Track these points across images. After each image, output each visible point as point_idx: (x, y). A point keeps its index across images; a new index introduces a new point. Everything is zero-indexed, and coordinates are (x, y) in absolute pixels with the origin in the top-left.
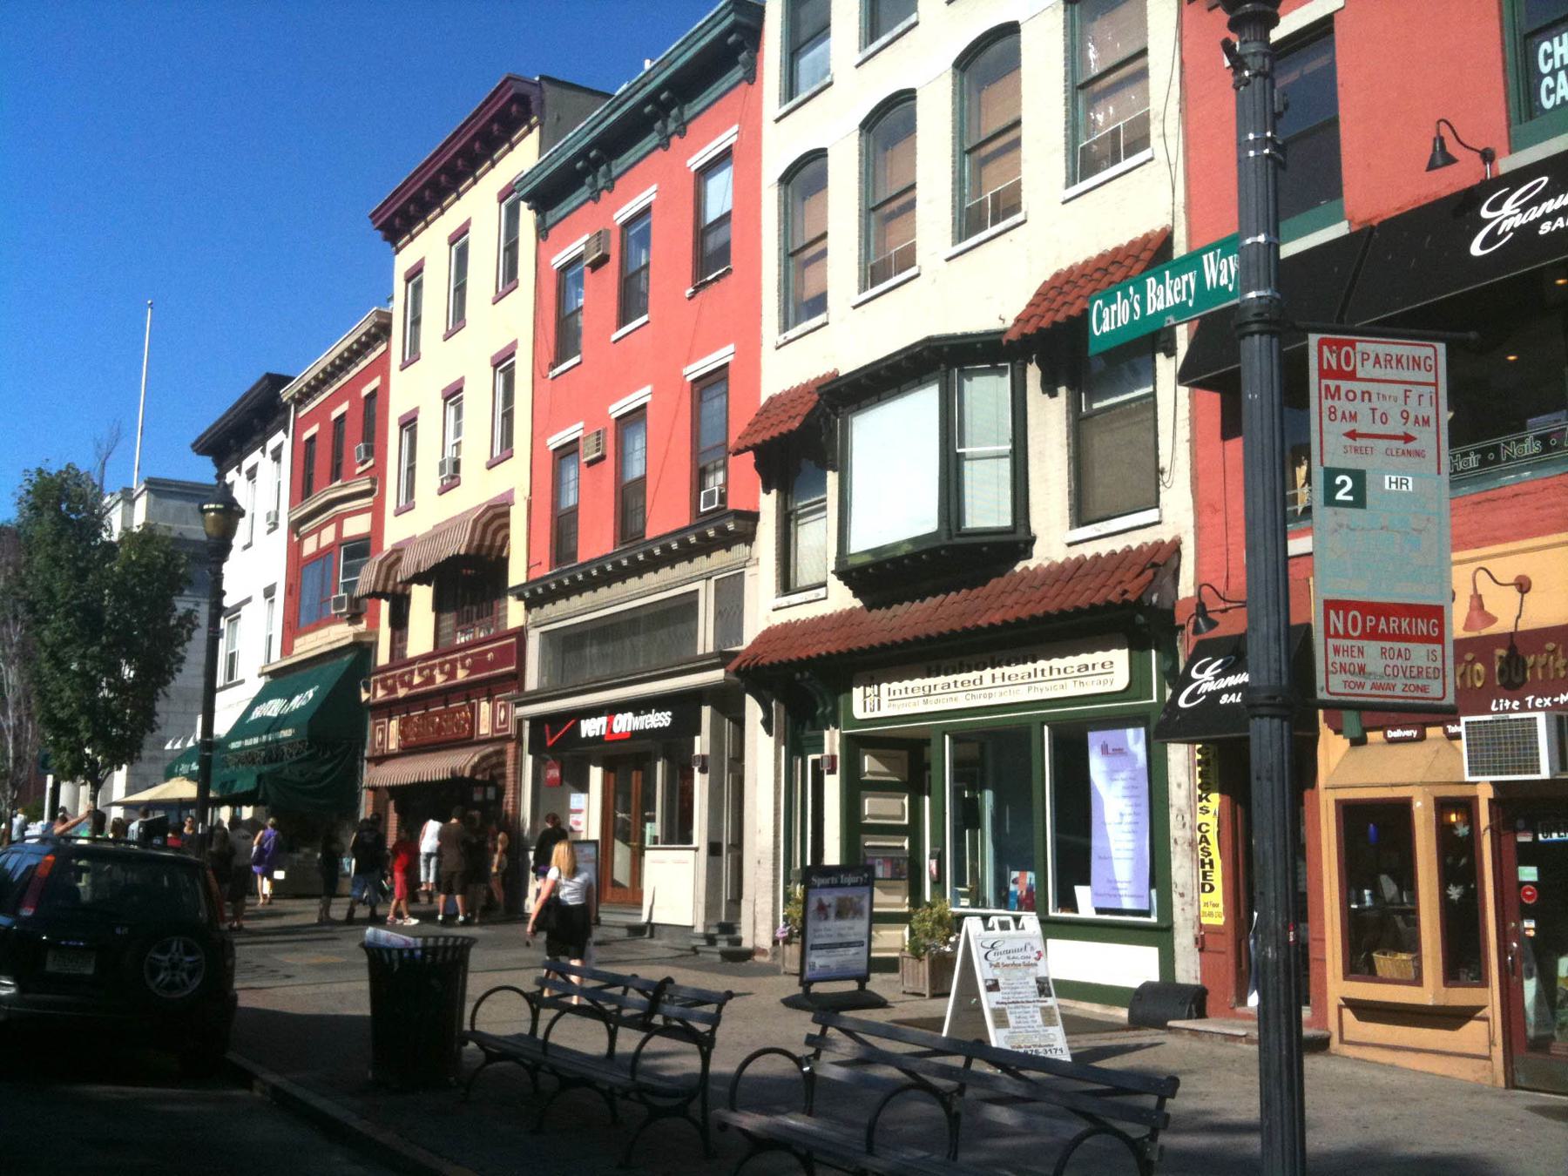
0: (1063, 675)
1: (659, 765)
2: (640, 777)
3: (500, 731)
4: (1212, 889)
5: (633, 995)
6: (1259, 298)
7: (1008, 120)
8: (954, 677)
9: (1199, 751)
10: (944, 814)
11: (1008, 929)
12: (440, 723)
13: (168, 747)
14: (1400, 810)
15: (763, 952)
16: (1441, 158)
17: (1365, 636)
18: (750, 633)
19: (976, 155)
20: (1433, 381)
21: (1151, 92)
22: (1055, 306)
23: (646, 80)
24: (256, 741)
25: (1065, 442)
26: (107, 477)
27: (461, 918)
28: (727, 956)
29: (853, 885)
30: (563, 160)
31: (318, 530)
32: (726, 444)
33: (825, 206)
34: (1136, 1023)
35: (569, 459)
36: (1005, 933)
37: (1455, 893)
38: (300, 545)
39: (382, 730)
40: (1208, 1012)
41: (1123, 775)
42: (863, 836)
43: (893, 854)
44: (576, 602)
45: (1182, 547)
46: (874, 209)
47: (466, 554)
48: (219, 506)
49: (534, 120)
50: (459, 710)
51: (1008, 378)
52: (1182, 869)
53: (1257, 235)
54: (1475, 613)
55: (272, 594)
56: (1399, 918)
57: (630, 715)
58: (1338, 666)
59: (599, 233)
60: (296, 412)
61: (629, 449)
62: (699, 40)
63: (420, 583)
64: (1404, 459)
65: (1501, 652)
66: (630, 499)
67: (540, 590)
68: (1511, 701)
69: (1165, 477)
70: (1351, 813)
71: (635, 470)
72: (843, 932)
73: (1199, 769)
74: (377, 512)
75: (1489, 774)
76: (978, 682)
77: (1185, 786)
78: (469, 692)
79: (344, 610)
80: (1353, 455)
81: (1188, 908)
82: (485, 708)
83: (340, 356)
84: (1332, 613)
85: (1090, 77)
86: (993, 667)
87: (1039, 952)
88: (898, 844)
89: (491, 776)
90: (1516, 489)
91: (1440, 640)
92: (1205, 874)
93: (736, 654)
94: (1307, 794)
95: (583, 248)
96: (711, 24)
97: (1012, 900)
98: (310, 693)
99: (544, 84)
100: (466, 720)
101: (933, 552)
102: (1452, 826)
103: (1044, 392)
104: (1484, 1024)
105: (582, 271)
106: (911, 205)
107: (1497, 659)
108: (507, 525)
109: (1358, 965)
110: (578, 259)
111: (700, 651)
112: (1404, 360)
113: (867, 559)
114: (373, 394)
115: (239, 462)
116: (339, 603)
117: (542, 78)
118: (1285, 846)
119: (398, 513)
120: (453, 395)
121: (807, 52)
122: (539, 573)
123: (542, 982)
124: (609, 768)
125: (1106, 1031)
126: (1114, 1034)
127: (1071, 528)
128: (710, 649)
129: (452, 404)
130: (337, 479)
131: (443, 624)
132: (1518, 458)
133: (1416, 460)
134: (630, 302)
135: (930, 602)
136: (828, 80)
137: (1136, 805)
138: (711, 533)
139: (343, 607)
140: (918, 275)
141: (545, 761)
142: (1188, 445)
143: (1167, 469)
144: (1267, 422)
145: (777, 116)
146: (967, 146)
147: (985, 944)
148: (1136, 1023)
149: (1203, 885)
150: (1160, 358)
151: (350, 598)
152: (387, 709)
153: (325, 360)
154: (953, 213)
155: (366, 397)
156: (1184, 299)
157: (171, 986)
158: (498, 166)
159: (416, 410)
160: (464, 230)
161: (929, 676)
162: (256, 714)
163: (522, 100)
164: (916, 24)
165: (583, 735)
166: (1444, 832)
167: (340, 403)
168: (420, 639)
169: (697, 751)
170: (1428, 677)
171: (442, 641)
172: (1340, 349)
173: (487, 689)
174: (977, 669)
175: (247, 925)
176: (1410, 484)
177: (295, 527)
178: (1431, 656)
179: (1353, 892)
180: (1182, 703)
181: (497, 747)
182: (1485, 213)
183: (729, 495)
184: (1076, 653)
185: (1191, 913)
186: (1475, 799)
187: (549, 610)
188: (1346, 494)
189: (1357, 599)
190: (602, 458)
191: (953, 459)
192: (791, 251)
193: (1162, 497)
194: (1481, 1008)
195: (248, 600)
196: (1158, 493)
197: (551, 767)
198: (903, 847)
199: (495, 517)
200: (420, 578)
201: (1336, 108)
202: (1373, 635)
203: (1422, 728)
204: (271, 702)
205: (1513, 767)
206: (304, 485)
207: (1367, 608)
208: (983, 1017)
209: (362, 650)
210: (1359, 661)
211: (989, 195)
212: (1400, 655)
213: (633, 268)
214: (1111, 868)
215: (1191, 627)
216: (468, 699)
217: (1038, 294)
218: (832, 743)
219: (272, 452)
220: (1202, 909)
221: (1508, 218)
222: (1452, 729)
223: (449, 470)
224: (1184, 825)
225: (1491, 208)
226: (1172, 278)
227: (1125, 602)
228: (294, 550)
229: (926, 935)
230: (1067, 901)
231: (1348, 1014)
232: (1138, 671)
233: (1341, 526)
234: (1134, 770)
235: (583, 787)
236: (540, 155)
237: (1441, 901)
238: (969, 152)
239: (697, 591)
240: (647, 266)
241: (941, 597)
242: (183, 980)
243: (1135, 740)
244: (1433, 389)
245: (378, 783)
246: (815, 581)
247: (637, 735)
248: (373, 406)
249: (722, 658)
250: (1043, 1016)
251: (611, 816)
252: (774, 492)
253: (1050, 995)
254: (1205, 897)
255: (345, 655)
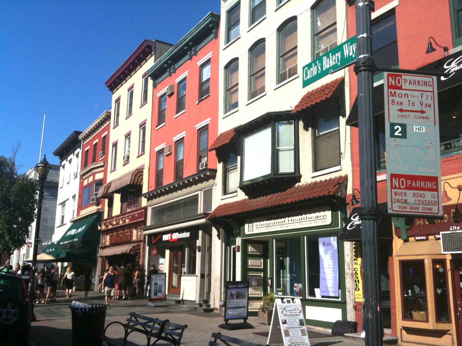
0: (310, 219)
1: (186, 249)
2: (181, 253)
3: (138, 239)
4: (359, 290)
5: (157, 326)
6: (364, 57)
7: (294, 46)
8: (276, 220)
9: (354, 244)
10: (273, 265)
11: (290, 303)
12: (121, 237)
13: (43, 244)
14: (421, 263)
15: (217, 309)
16: (431, 49)
17: (406, 188)
18: (214, 207)
19: (284, 57)
20: (432, 90)
21: (338, 35)
22: (307, 102)
23: (185, 39)
24: (67, 242)
25: (311, 145)
26: (16, 158)
27: (124, 298)
28: (205, 310)
29: (242, 288)
30: (161, 64)
31: (88, 178)
32: (208, 148)
33: (238, 75)
34: (334, 334)
35: (161, 154)
36: (289, 304)
37: (439, 291)
38: (83, 183)
39: (105, 239)
40: (358, 331)
41: (330, 252)
42: (248, 272)
43: (258, 278)
44: (162, 198)
45: (348, 178)
46: (253, 75)
47: (130, 184)
48: (43, 165)
49: (153, 53)
50: (128, 232)
51: (293, 125)
52: (349, 283)
53: (363, 34)
54: (444, 197)
55: (75, 197)
56: (420, 300)
57: (177, 233)
58: (396, 200)
59: (171, 86)
60: (83, 142)
61: (179, 150)
62: (201, 26)
63: (117, 193)
64: (422, 120)
65: (453, 210)
66: (179, 166)
67: (151, 195)
68: (457, 227)
69: (342, 156)
70: (405, 265)
71: (180, 157)
72: (239, 303)
73: (354, 250)
74: (105, 172)
75: (450, 251)
76: (284, 222)
77: (350, 256)
78: (130, 226)
79: (95, 202)
80: (401, 118)
81: (351, 296)
82: (135, 231)
83: (96, 125)
84: (394, 179)
85: (319, 31)
86: (288, 217)
87: (300, 311)
88: (260, 275)
89: (136, 253)
90: (457, 157)
91: (437, 190)
92: (356, 285)
93: (209, 214)
94: (390, 258)
95: (166, 91)
96: (204, 21)
97: (295, 293)
98: (84, 227)
99: (156, 42)
100: (129, 235)
101: (269, 180)
102: (438, 269)
103: (304, 130)
104: (450, 336)
105: (166, 97)
106: (264, 74)
107: (452, 213)
108: (142, 175)
109: (407, 316)
110: (165, 94)
111: (199, 213)
112: (421, 82)
113: (249, 183)
114: (105, 136)
115: (67, 158)
116: (93, 200)
117: (155, 40)
118: (376, 271)
119: (111, 172)
120: (128, 136)
121: (233, 28)
122: (151, 189)
123: (129, 320)
124: (171, 250)
125: (324, 337)
126: (326, 338)
127: (313, 172)
128: (202, 212)
129: (128, 139)
130: (94, 162)
131: (123, 206)
132: (457, 147)
133: (426, 120)
134: (180, 106)
135: (269, 196)
136: (239, 36)
137: (334, 262)
138: (202, 176)
139: (94, 201)
140: (266, 95)
141: (152, 248)
142: (350, 145)
143: (343, 153)
144: (367, 105)
145: (224, 48)
146: (281, 55)
147: (282, 308)
148: (334, 334)
149: (356, 288)
150: (341, 118)
151: (96, 198)
152: (106, 232)
153: (91, 127)
154: (277, 75)
155: (103, 137)
156: (337, 62)
157: (7, 320)
158: (142, 67)
159: (117, 141)
160: (132, 87)
161: (268, 220)
162: (68, 234)
163: (149, 47)
164: (265, 18)
165: (163, 240)
166: (435, 271)
167: (95, 140)
168: (116, 211)
169: (197, 245)
170: (432, 205)
171: (123, 211)
172: (396, 77)
173: (136, 225)
174: (283, 218)
175: (57, 299)
176: (424, 130)
177: (82, 176)
178: (433, 197)
179: (405, 291)
180: (348, 228)
181: (138, 244)
182: (445, 67)
183: (208, 164)
184: (314, 212)
185: (352, 298)
186: (445, 260)
187: (154, 201)
188: (399, 133)
189: (403, 174)
190: (171, 154)
191: (275, 151)
192: (227, 89)
193: (341, 162)
194: (449, 331)
195: (68, 199)
196: (340, 161)
197: (154, 250)
198: (261, 276)
199: (139, 173)
200: (117, 191)
201: (396, 37)
202: (410, 188)
203: (427, 236)
204: (72, 230)
205: (458, 249)
206: (85, 164)
207: (407, 177)
208: (281, 332)
209: (99, 214)
210: (405, 198)
211: (287, 69)
212: (421, 196)
213: (181, 96)
214: (326, 283)
215: (351, 203)
216: (130, 229)
217: (302, 99)
218: (238, 242)
219: (76, 155)
220: (356, 296)
221: (453, 68)
222: (437, 236)
223: (126, 159)
224: (350, 269)
225: (447, 65)
226: (332, 55)
227: (330, 195)
228: (81, 183)
229: (267, 304)
230: (312, 293)
231: (404, 332)
232: (334, 218)
233: (397, 145)
234: (333, 251)
235: (164, 256)
236: (155, 63)
237: (434, 293)
238: (281, 56)
239: (198, 194)
240: (185, 95)
241: (272, 195)
242: (11, 318)
243: (333, 240)
244: (432, 93)
245: (102, 255)
246: (234, 191)
247: (179, 240)
248: (105, 140)
249: (205, 215)
250: (301, 332)
251: (172, 265)
252: (222, 163)
253: (304, 325)
254: (356, 292)
255: (94, 215)
